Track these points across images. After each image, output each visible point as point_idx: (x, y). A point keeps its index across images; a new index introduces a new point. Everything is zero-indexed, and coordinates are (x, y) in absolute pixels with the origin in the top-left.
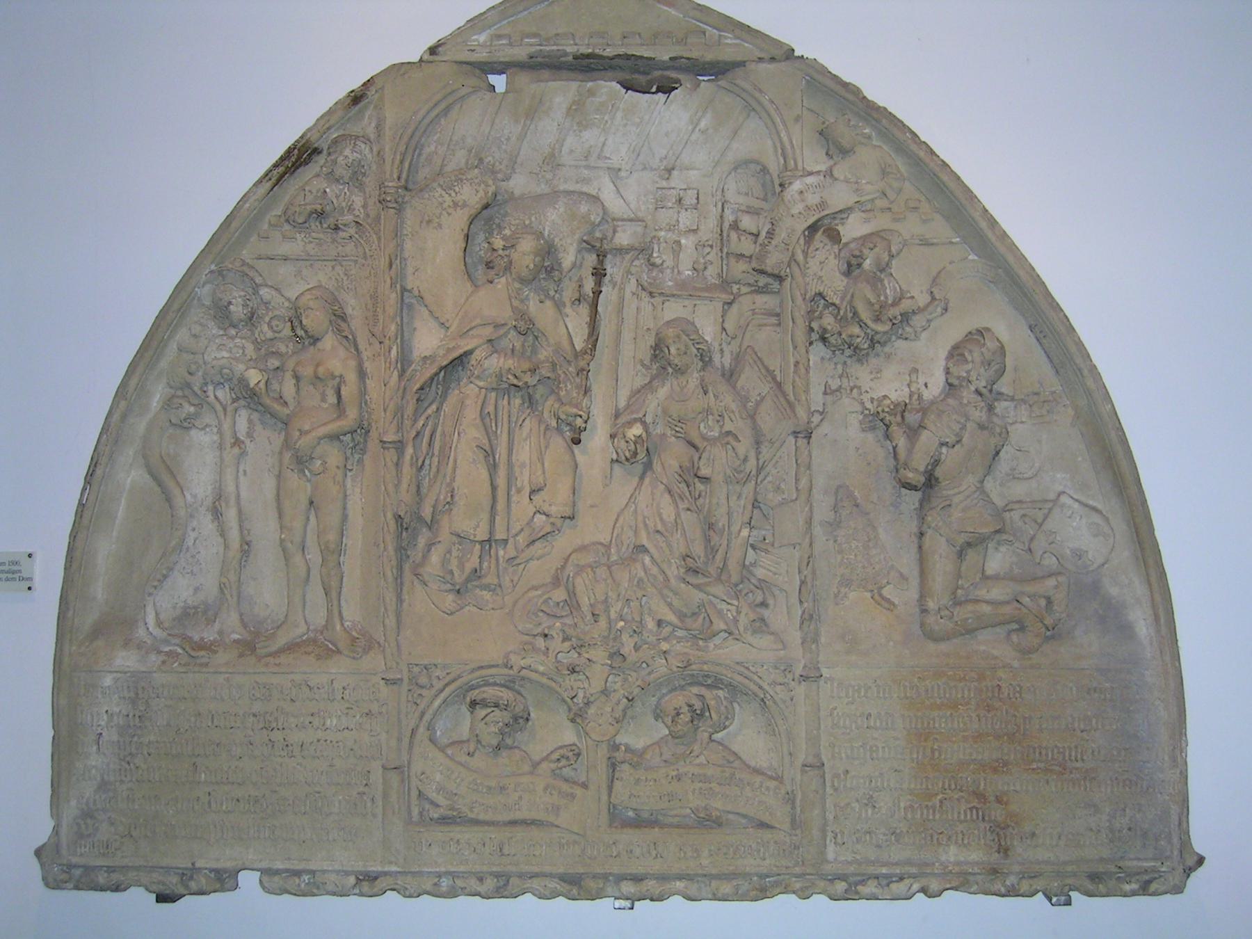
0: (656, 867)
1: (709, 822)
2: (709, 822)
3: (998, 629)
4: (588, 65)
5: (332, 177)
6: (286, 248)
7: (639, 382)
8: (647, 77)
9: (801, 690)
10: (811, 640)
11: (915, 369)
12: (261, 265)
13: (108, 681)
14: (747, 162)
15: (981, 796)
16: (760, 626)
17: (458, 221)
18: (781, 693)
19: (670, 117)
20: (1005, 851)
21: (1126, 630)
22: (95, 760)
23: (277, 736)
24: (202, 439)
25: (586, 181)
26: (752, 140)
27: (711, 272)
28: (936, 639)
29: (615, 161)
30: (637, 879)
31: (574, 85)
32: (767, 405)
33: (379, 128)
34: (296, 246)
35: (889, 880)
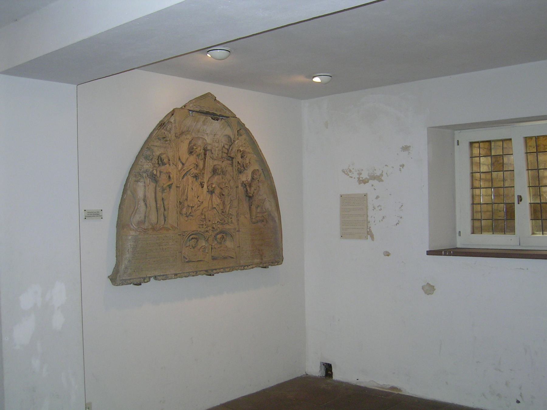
0: (219, 267)
1: (225, 258)
2: (225, 258)
3: (528, 141)
4: (207, 113)
5: (166, 130)
6: (156, 144)
7: (210, 176)
8: (215, 117)
9: (237, 233)
10: (238, 224)
11: (246, 177)
12: (152, 147)
13: (130, 238)
14: (226, 135)
15: (259, 250)
16: (232, 223)
17: (188, 141)
18: (234, 234)
19: (217, 125)
20: (262, 259)
21: (275, 221)
22: (128, 256)
23: (161, 247)
24: (141, 184)
25: (203, 135)
26: (228, 131)
27: (220, 156)
28: (254, 223)
29: (207, 132)
30: (216, 270)
31: (204, 117)
32: (232, 181)
33: (175, 120)
34: (158, 143)
35: (248, 266)
